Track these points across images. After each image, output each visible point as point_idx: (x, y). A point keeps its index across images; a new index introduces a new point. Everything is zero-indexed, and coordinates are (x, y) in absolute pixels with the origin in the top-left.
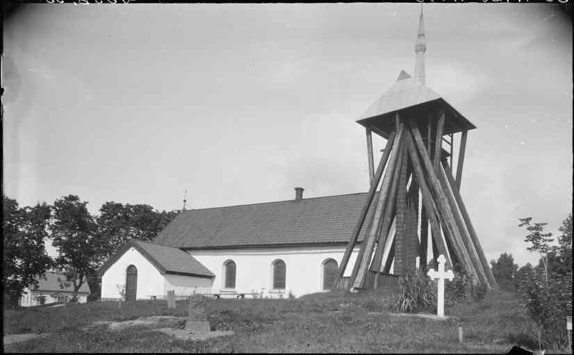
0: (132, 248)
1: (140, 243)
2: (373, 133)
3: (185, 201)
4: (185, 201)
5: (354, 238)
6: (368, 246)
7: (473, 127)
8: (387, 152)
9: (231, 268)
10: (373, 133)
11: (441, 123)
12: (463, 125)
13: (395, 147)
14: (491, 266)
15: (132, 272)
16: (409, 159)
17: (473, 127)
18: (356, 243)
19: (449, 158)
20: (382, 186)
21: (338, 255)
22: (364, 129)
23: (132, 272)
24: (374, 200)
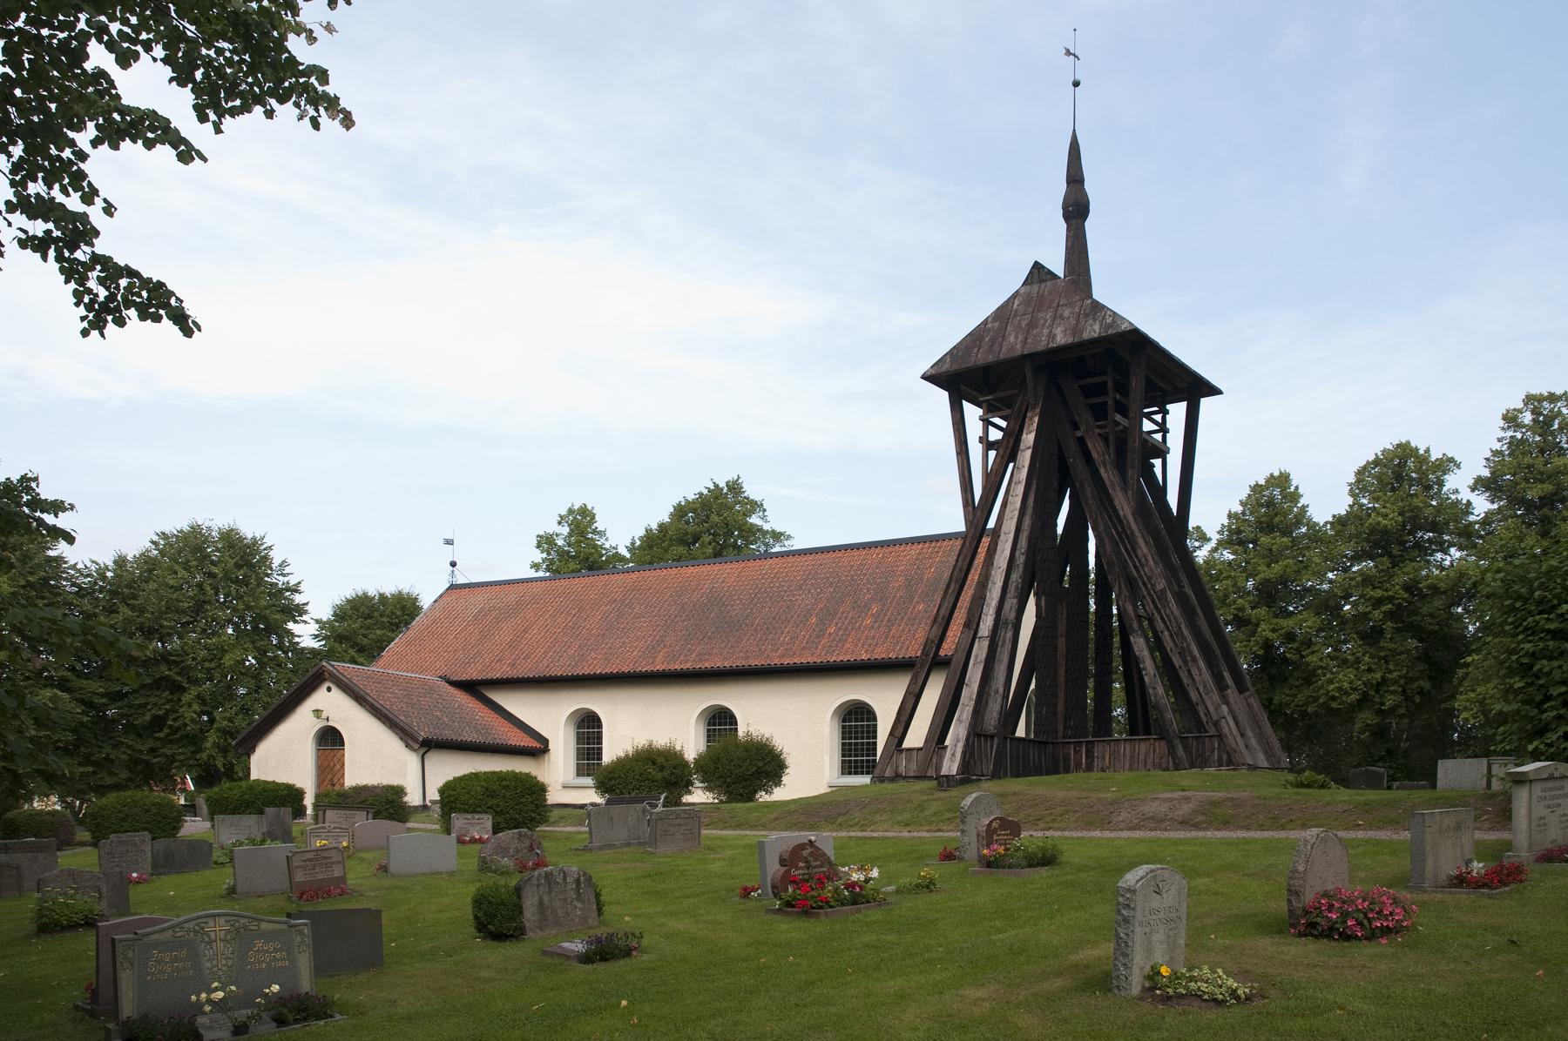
0: (327, 684)
1: (344, 668)
2: (965, 403)
3: (453, 564)
4: (453, 564)
5: (197, 810)
6: (1256, 836)
7: (1213, 391)
8: (1008, 450)
9: (588, 728)
10: (965, 403)
11: (1136, 384)
12: (1194, 388)
13: (1029, 438)
14: (548, 574)
15: (330, 739)
16: (1062, 460)
17: (1213, 391)
18: (939, 663)
19: (1157, 462)
20: (1006, 513)
21: (884, 699)
22: (942, 396)
23: (330, 739)
24: (974, 576)
